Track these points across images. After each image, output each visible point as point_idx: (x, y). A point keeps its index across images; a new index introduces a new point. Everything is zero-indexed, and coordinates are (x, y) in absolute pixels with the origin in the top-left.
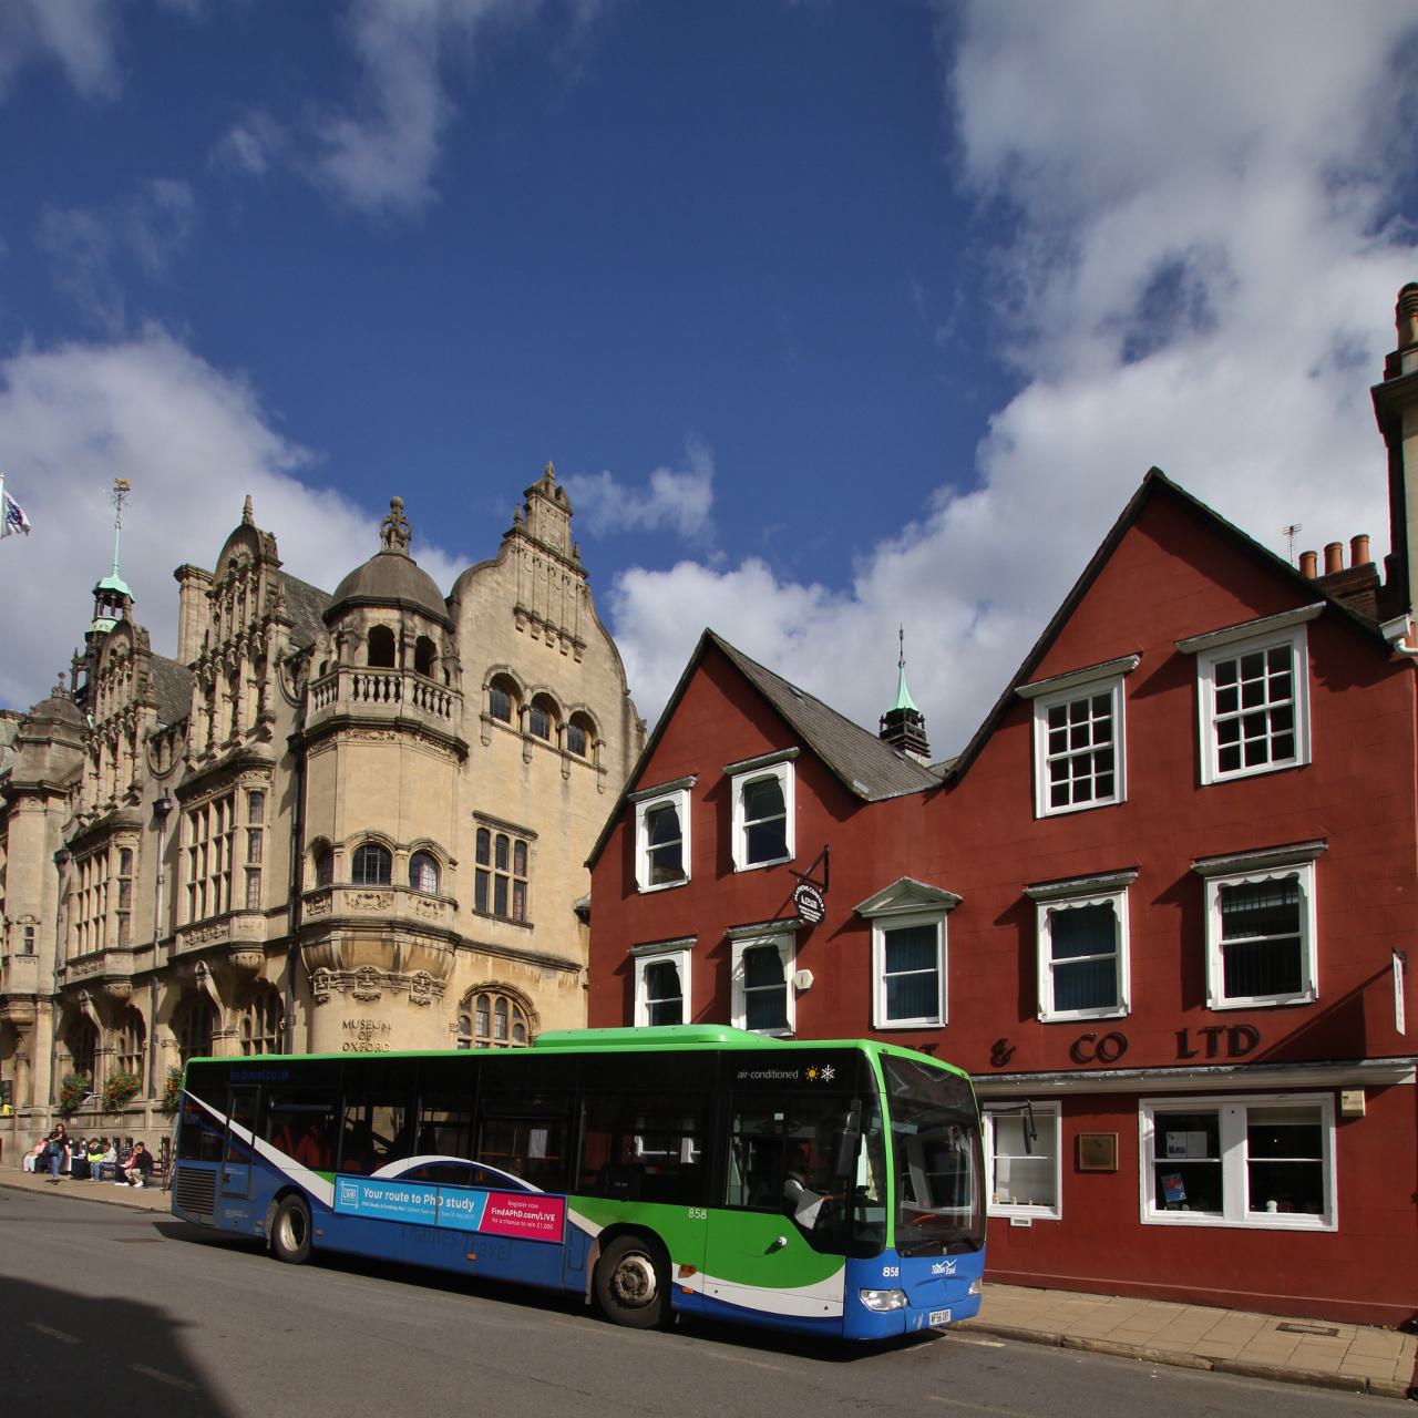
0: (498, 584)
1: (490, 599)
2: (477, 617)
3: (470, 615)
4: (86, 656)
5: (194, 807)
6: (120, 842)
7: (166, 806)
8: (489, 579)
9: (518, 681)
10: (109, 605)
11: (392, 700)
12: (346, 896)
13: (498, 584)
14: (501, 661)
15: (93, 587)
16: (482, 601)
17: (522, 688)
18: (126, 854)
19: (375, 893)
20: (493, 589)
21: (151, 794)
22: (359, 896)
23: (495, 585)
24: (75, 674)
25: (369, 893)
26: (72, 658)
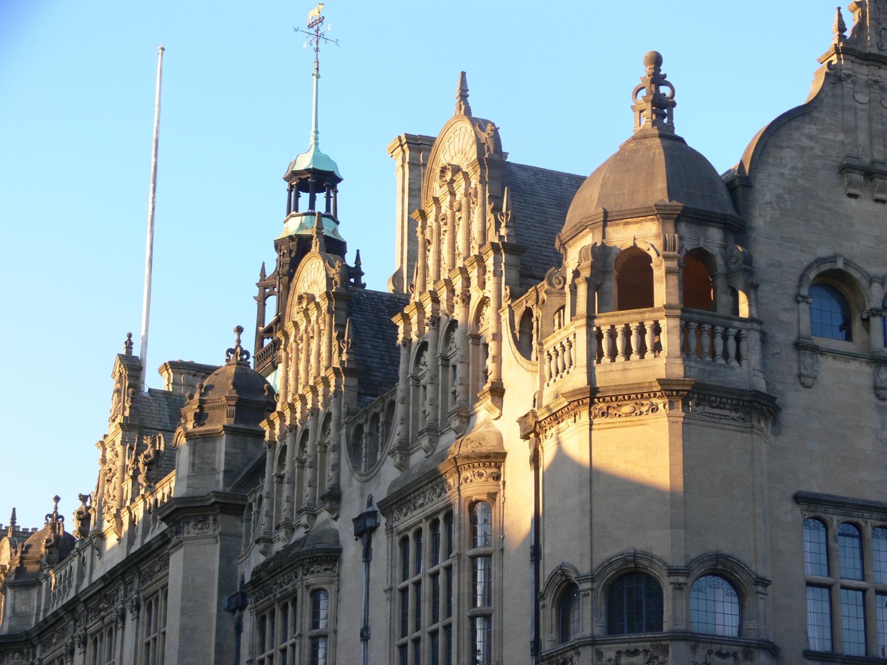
0: (810, 137)
1: (800, 166)
2: (779, 198)
3: (768, 198)
4: (277, 273)
5: (402, 527)
6: (311, 579)
7: (369, 523)
8: (796, 135)
9: (857, 275)
10: (306, 191)
11: (649, 355)
12: (599, 654)
13: (810, 137)
14: (824, 252)
15: (284, 172)
16: (786, 171)
17: (864, 283)
18: (315, 594)
19: (640, 646)
20: (803, 149)
21: (353, 507)
22: (619, 653)
23: (806, 143)
24: (262, 301)
25: (633, 646)
26: (257, 279)
